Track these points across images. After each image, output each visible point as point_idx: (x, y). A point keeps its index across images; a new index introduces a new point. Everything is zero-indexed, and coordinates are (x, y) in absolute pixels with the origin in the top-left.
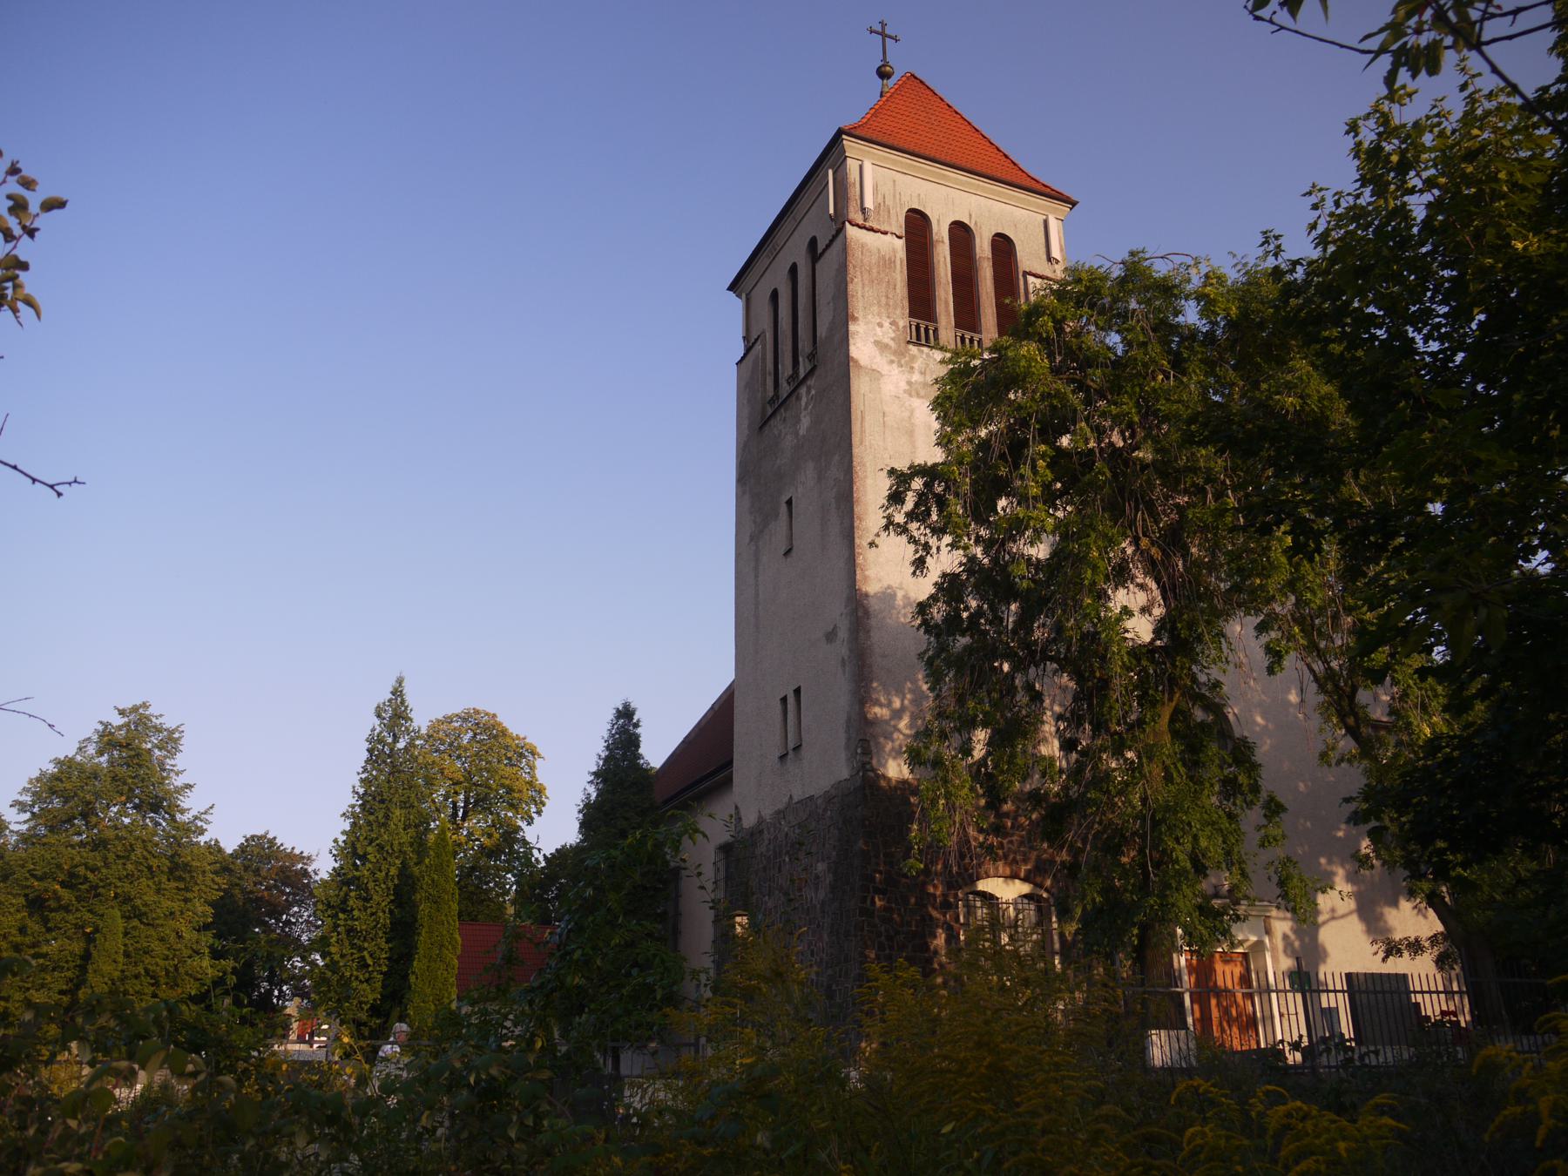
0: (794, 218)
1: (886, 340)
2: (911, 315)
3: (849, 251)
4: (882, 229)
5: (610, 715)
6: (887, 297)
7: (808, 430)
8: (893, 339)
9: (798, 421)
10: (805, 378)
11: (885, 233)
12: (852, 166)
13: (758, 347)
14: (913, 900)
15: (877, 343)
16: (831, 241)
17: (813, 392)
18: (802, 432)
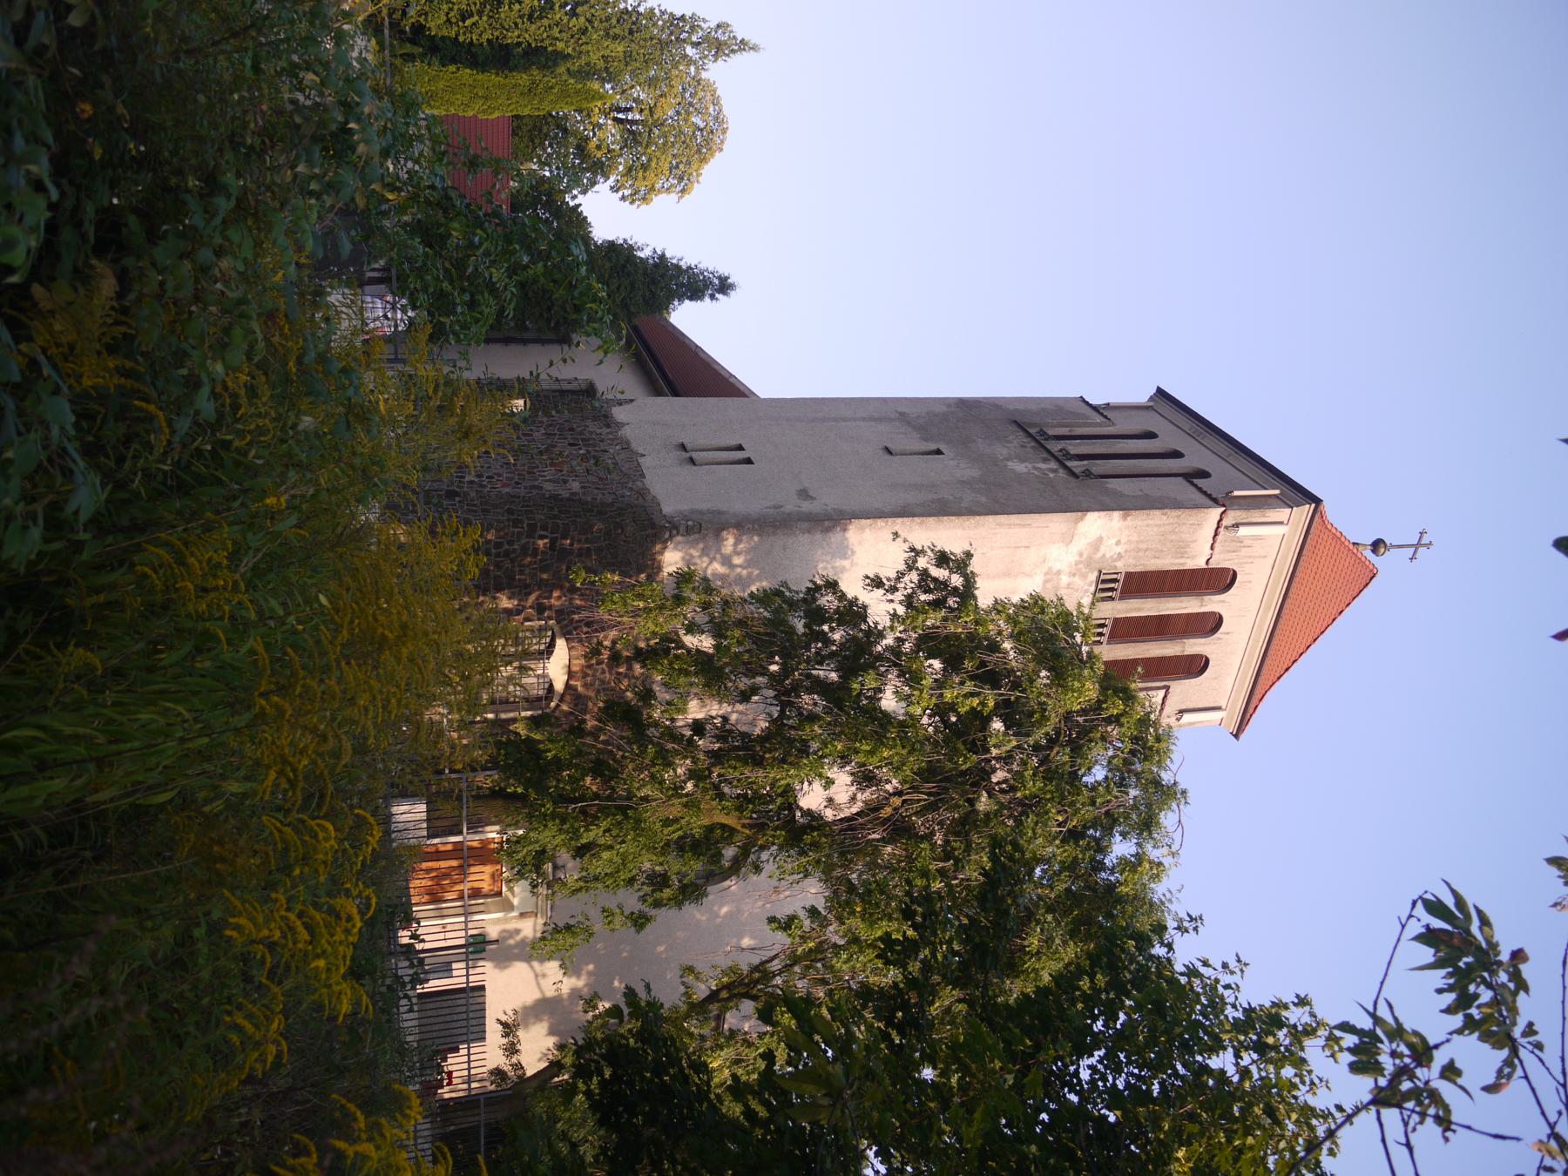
0: (1230, 455)
1: (1103, 549)
3: (1195, 511)
5: (723, 270)
7: (1013, 471)
8: (1104, 555)
9: (1022, 461)
10: (1066, 467)
13: (1099, 419)
14: (545, 576)
15: (1100, 540)
17: (1051, 475)
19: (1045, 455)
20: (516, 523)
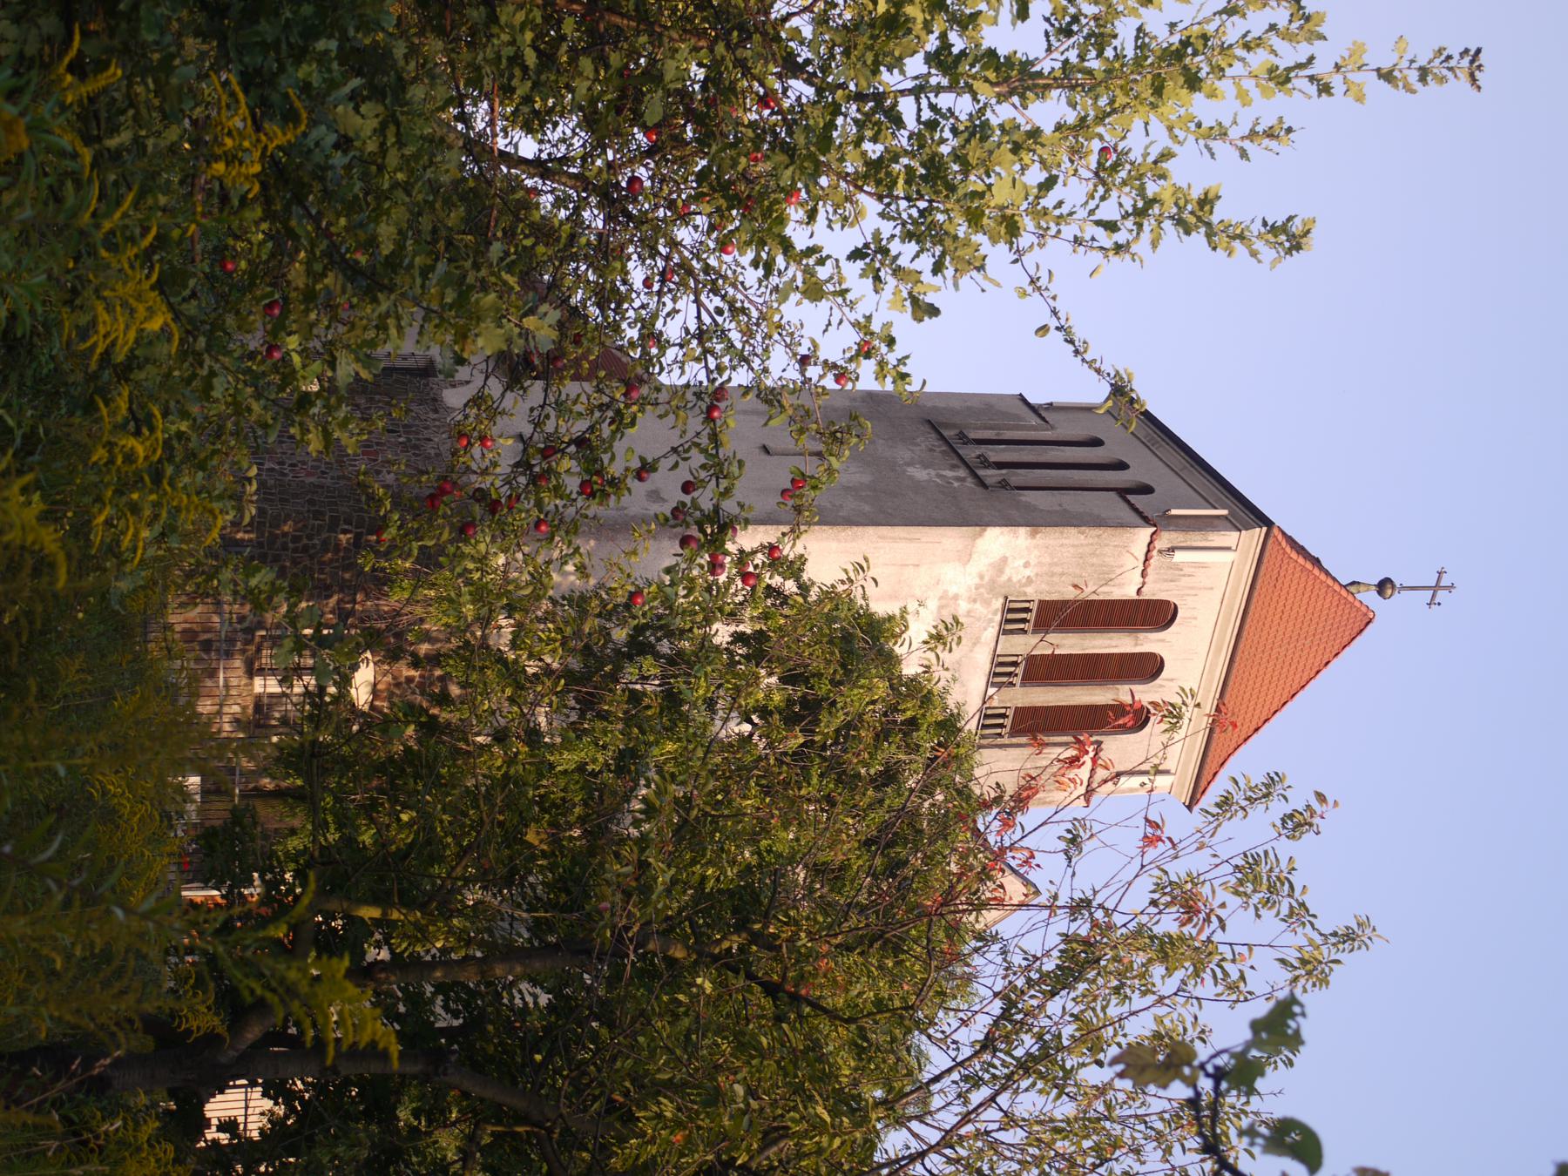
1: (1008, 572)
2: (1041, 602)
3: (1120, 530)
4: (1149, 570)
6: (1062, 574)
7: (911, 478)
8: (1010, 579)
9: (926, 467)
10: (976, 476)
11: (1144, 574)
12: (1230, 538)
13: (1034, 420)
14: (347, 576)
15: (1004, 560)
16: (1136, 510)
17: (956, 484)
18: (911, 470)
19: (956, 461)
20: (318, 515)
